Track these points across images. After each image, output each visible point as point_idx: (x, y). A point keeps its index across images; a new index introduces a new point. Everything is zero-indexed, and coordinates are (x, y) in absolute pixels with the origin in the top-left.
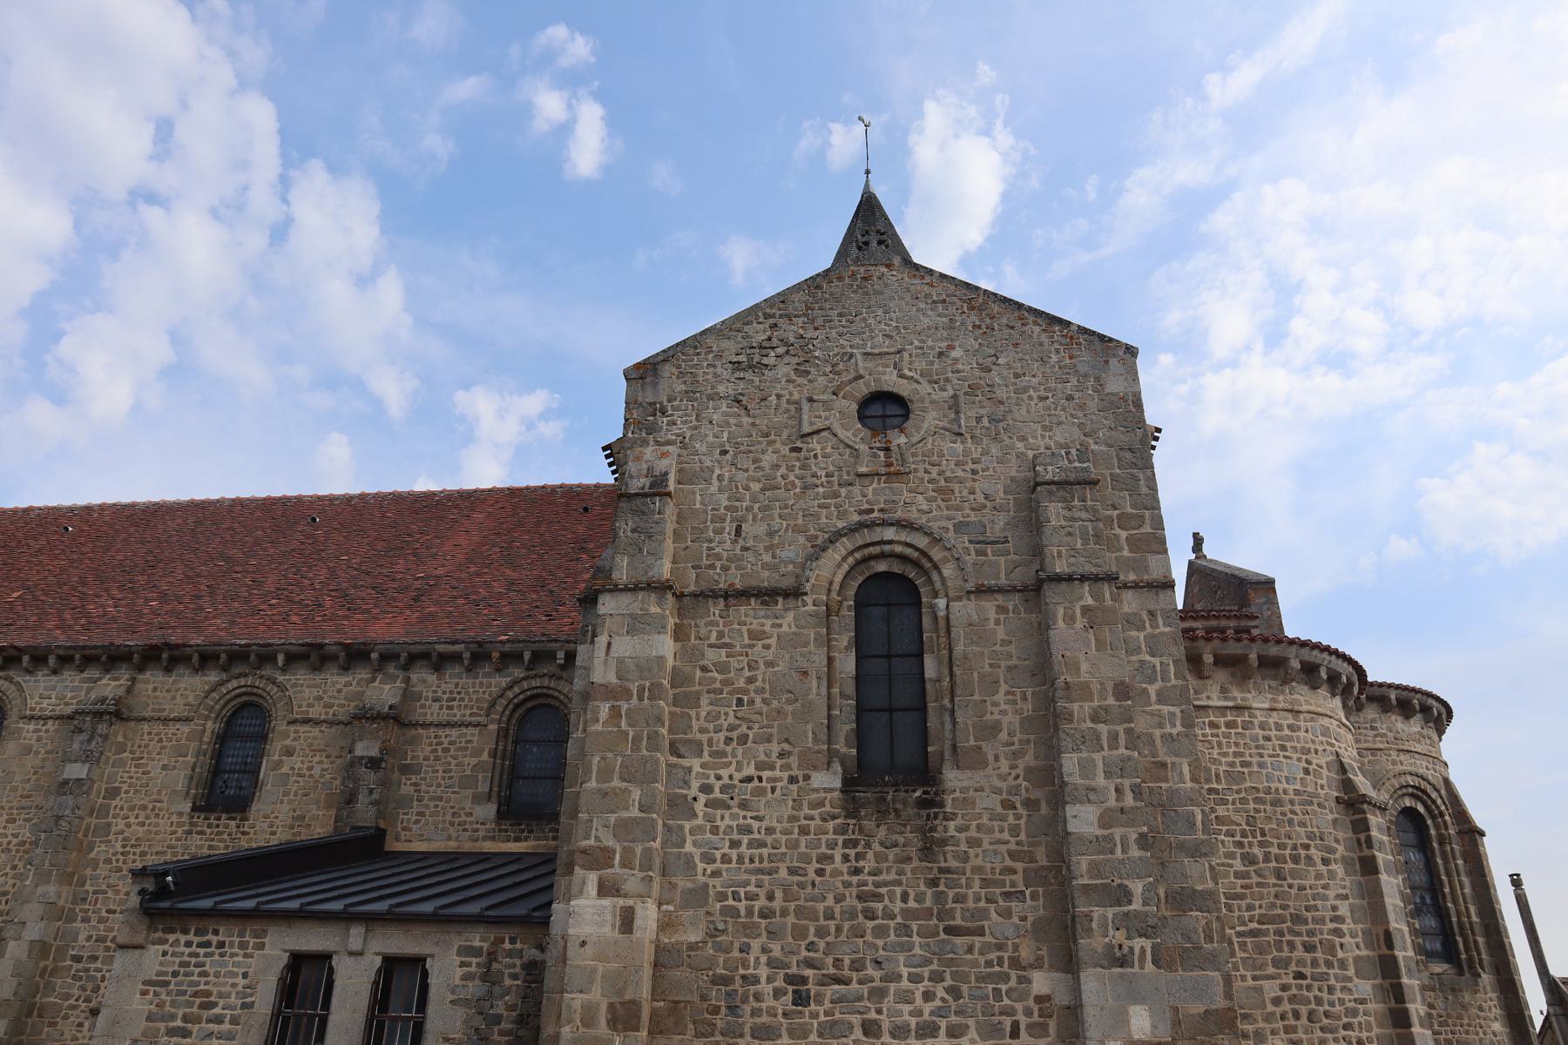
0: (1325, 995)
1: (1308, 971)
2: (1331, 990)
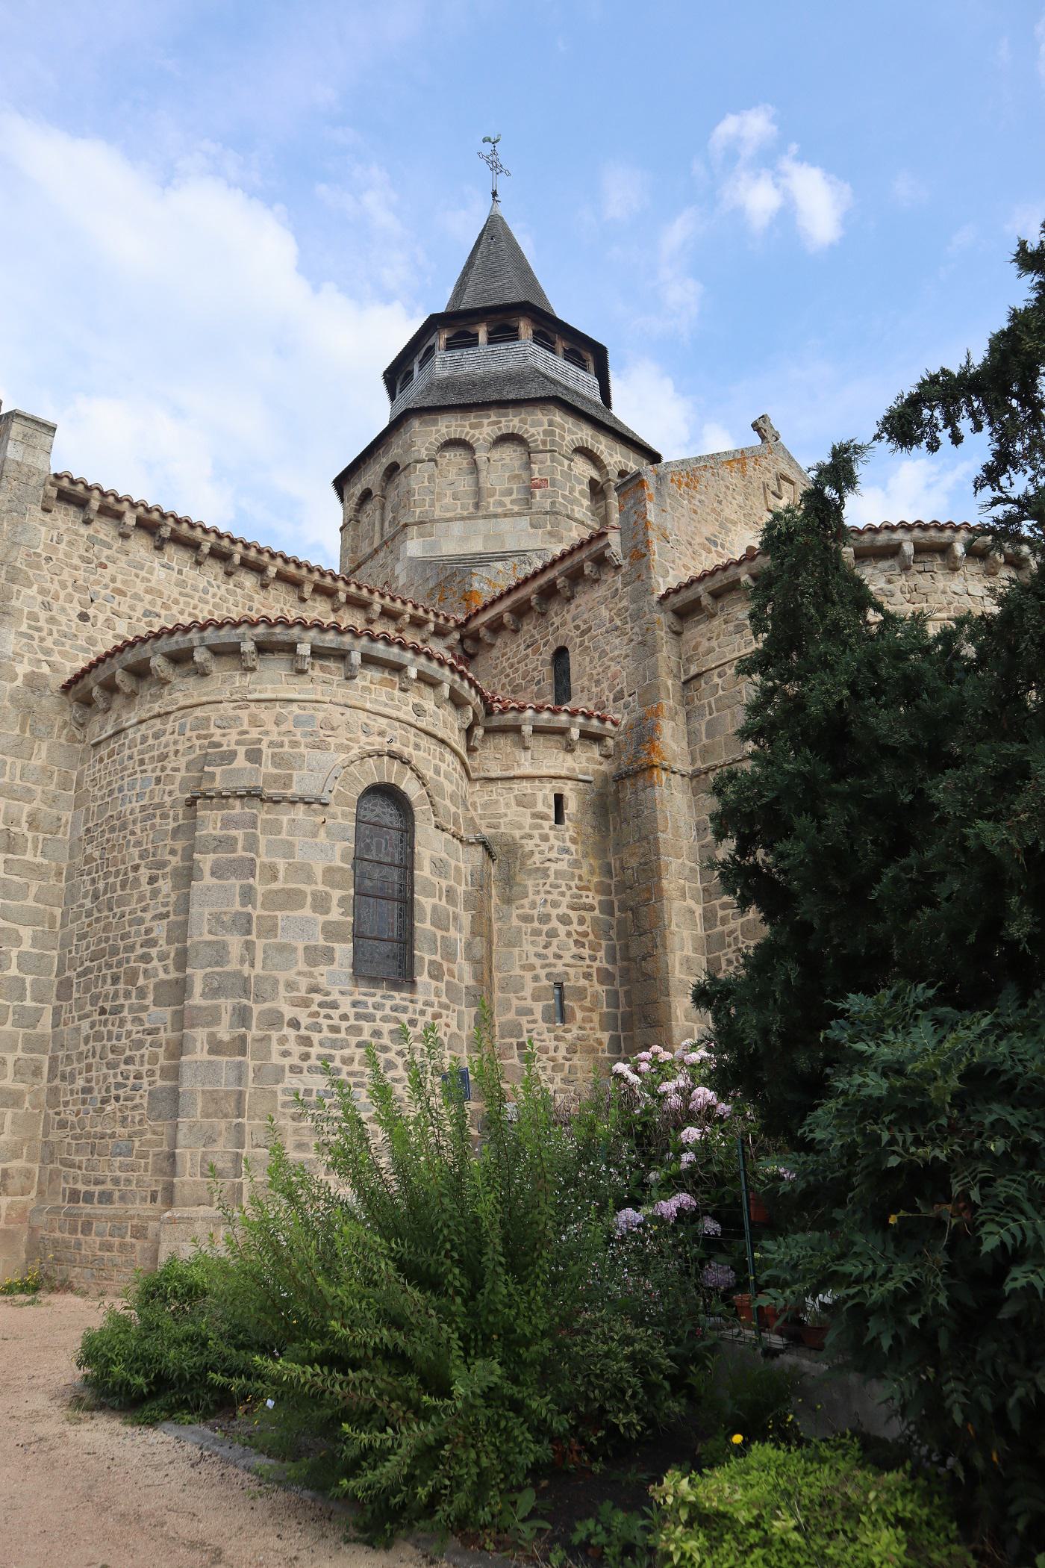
1: (108, 1006)
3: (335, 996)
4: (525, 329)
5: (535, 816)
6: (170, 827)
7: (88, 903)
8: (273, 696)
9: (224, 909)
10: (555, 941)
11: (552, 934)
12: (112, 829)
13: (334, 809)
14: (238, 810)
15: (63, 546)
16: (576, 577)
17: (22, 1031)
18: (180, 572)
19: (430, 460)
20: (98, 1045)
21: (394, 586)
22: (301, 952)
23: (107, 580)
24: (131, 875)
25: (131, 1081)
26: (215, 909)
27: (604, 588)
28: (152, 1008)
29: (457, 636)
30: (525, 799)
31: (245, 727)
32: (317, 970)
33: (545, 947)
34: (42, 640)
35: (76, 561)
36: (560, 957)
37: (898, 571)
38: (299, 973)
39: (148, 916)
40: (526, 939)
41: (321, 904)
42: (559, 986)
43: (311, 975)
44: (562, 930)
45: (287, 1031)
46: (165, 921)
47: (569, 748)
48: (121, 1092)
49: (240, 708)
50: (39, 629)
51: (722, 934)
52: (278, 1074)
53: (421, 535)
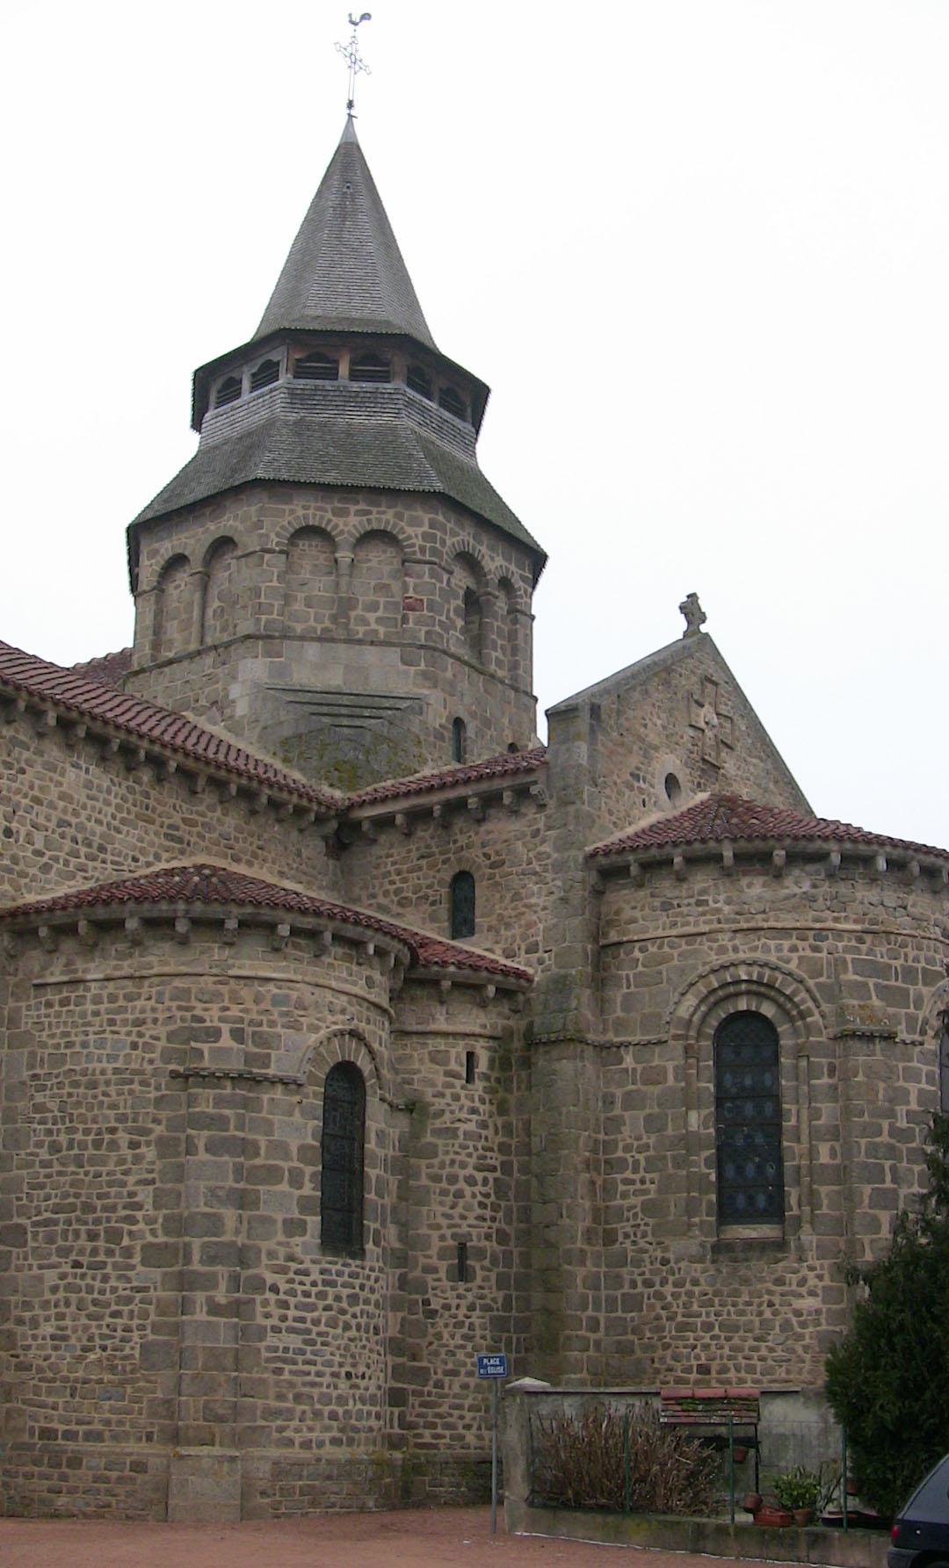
0: (97, 1284)
1: (85, 1260)
2: (105, 1279)
4: (400, 363)
6: (152, 1096)
7: (44, 1154)
10: (461, 1202)
11: (459, 1194)
12: (76, 1084)
14: (229, 1091)
16: (491, 800)
18: (87, 770)
19: (281, 552)
20: (73, 1297)
21: (228, 711)
22: (280, 1224)
23: (25, 789)
24: (107, 1137)
26: (212, 1183)
27: (524, 821)
28: (140, 1268)
29: (334, 824)
30: (440, 1056)
31: (226, 1004)
33: (452, 1208)
36: (463, 1217)
37: (823, 876)
38: (279, 1244)
39: (131, 1179)
40: (435, 1198)
41: (296, 1181)
42: (462, 1248)
43: (288, 1245)
44: (468, 1190)
45: (269, 1295)
46: (151, 1188)
47: (483, 1005)
48: (108, 1342)
49: (220, 983)
51: (621, 1207)
52: (261, 1333)
53: (268, 654)
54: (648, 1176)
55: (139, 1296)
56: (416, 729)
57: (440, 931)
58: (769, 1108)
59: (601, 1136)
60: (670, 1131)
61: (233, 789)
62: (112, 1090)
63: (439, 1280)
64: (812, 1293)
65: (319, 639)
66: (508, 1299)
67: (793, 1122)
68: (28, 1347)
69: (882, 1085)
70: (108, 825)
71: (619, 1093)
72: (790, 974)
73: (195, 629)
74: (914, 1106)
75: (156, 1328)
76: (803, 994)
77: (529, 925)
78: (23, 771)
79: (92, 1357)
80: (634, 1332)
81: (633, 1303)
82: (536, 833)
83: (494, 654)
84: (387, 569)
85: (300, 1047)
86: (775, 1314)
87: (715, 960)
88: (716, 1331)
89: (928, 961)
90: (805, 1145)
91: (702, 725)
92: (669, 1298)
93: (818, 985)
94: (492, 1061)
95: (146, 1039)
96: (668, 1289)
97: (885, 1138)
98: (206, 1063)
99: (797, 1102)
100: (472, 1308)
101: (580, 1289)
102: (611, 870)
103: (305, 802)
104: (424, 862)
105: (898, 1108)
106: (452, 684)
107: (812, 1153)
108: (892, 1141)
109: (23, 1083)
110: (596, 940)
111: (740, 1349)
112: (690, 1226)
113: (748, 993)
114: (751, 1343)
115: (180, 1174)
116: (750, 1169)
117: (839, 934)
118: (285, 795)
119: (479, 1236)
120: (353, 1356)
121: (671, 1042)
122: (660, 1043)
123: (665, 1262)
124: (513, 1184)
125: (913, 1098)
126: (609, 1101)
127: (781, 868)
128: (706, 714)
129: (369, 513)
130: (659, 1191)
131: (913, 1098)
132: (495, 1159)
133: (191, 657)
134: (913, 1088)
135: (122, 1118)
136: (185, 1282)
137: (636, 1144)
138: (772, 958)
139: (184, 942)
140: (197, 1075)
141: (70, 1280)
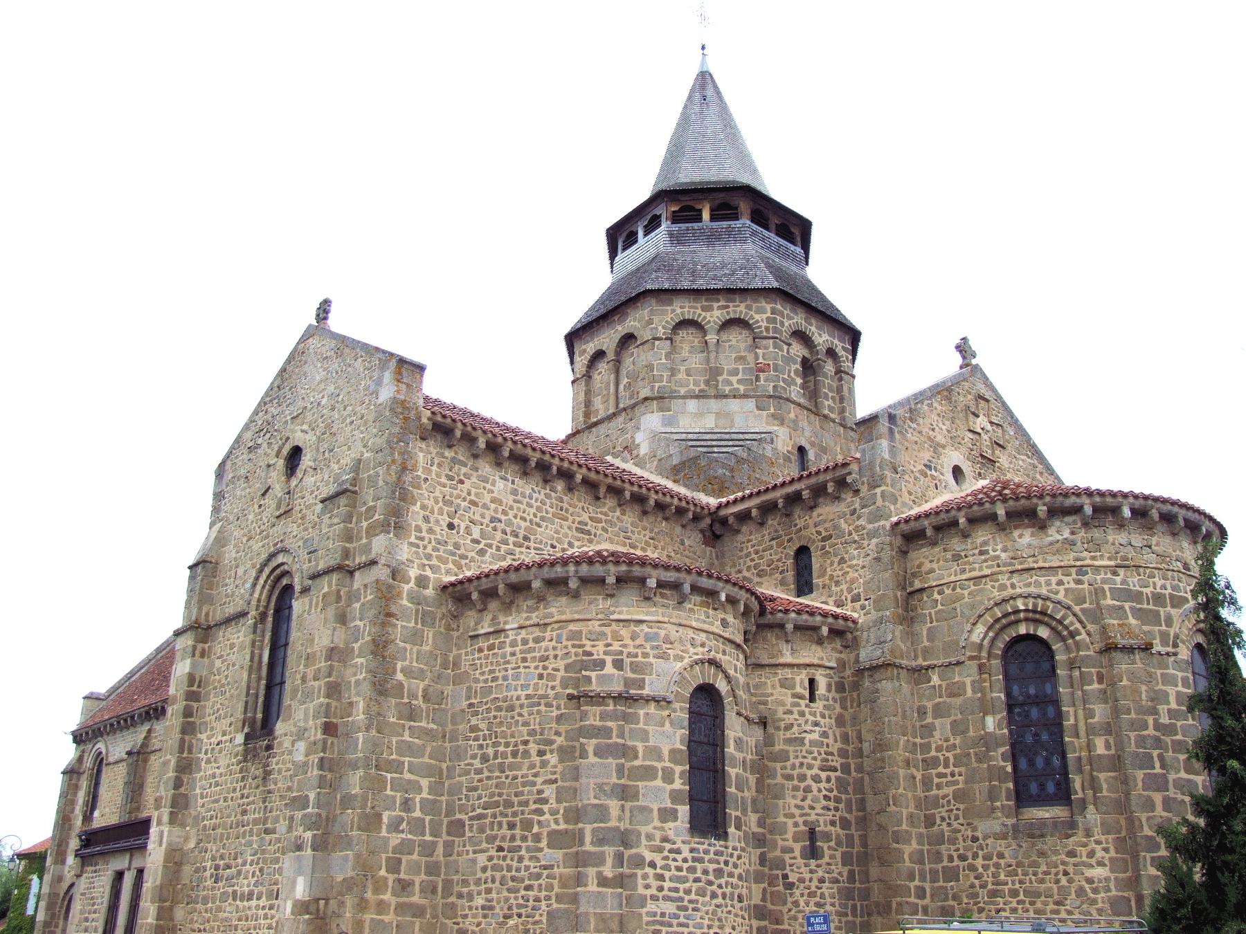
0: (515, 864)
1: (505, 845)
2: (521, 859)
3: (679, 845)
5: (794, 696)
6: (554, 714)
7: (477, 763)
8: (629, 617)
9: (605, 781)
10: (810, 796)
11: (807, 790)
12: (499, 709)
13: (677, 705)
15: (434, 468)
17: (424, 859)
18: (513, 482)
20: (498, 875)
22: (655, 813)
23: (464, 494)
24: (521, 748)
25: (531, 903)
26: (599, 781)
28: (546, 850)
29: (708, 521)
31: (609, 641)
32: (667, 825)
33: (803, 800)
34: (425, 547)
35: (444, 480)
38: (655, 828)
39: (539, 780)
40: (788, 793)
41: (668, 777)
43: (662, 829)
44: (814, 786)
45: (648, 870)
47: (820, 642)
48: (523, 911)
50: (422, 539)
51: (937, 797)
52: (643, 901)
54: (957, 770)
55: (545, 872)
56: (769, 453)
57: (788, 591)
58: (1051, 711)
59: (918, 740)
60: (971, 733)
61: (627, 495)
62: (525, 711)
63: (794, 858)
64: (1101, 864)
65: (697, 397)
66: (851, 873)
67: (1072, 721)
68: (466, 916)
69: (1144, 688)
70: (531, 521)
71: (929, 705)
72: (1059, 603)
73: (612, 399)
74: (1174, 706)
75: (559, 899)
76: (1071, 618)
77: (851, 582)
78: (462, 482)
79: (511, 922)
80: (954, 898)
81: (952, 874)
82: (853, 512)
83: (826, 403)
84: (742, 346)
85: (669, 674)
86: (1070, 881)
87: (997, 595)
88: (1022, 897)
89: (1173, 588)
90: (1083, 740)
91: (979, 430)
92: (981, 870)
93: (1082, 610)
94: (829, 686)
95: (549, 671)
96: (979, 862)
97: (1151, 731)
98: (595, 687)
99: (1074, 705)
100: (822, 881)
101: (908, 864)
102: (911, 536)
103: (684, 504)
104: (774, 542)
105: (1160, 707)
106: (795, 422)
107: (1090, 746)
108: (1158, 734)
109: (463, 711)
110: (904, 588)
111: (1043, 912)
112: (993, 809)
113: (1026, 619)
114: (1052, 906)
115: (576, 774)
116: (1039, 762)
117: (1097, 569)
118: (668, 499)
119: (825, 822)
120: (720, 920)
121: (968, 663)
122: (959, 663)
123: (975, 839)
124: (851, 781)
125: (1172, 699)
126: (922, 712)
127: (1044, 520)
128: (981, 422)
129: (728, 307)
130: (966, 782)
131: (1172, 699)
132: (836, 762)
133: (610, 418)
134: (1171, 691)
135: (532, 733)
136: (580, 860)
137: (945, 745)
138: (1044, 591)
139: (576, 595)
140: (586, 696)
141: (495, 861)
